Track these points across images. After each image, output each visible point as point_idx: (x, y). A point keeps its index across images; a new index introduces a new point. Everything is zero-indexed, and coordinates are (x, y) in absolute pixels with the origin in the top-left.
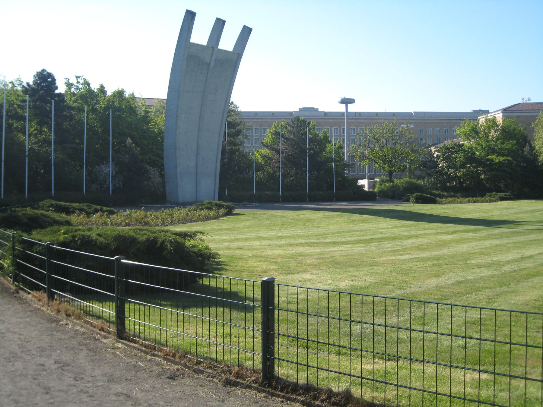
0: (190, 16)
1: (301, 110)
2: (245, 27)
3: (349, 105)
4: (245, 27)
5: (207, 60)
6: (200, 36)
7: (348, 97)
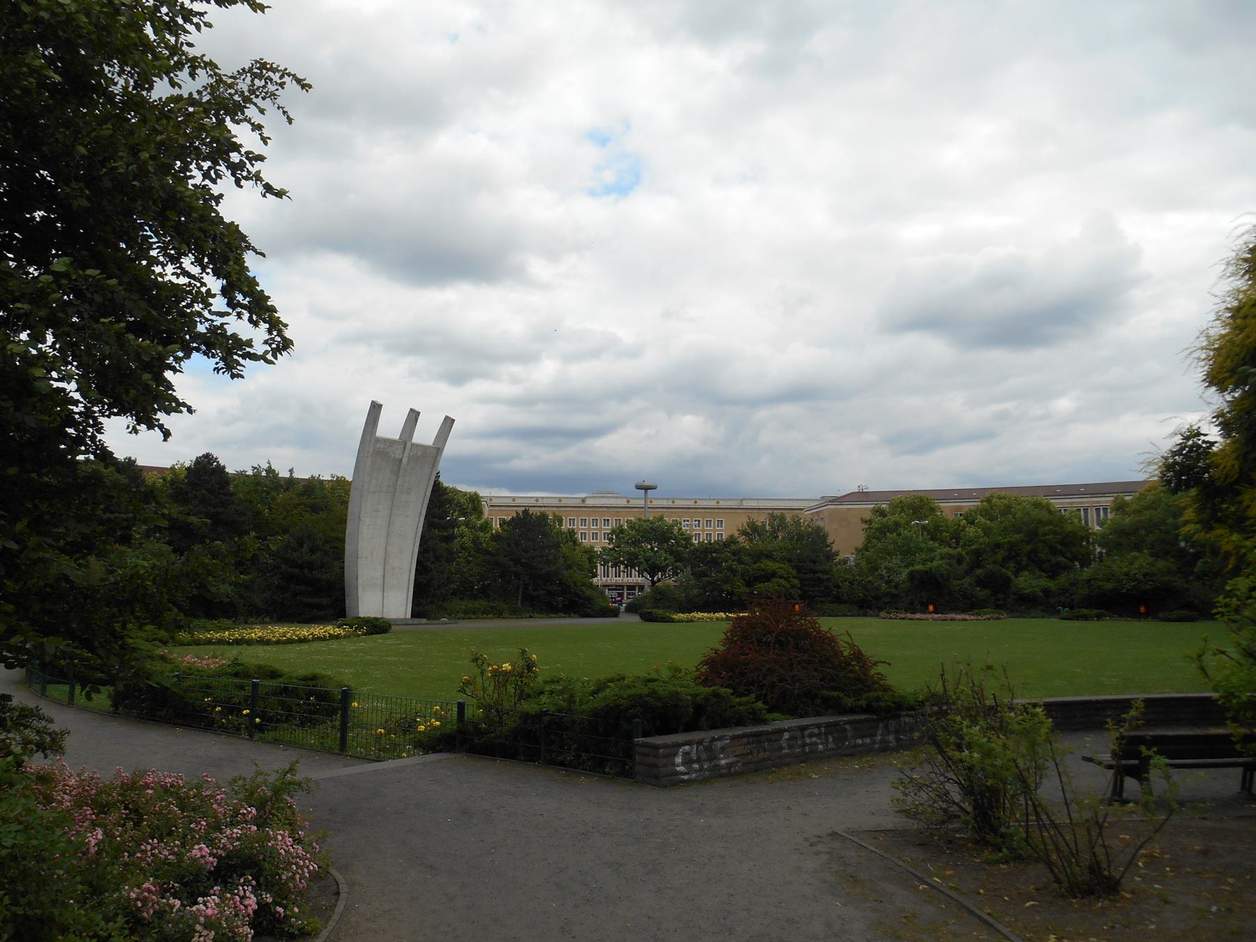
2: (447, 418)
4: (447, 418)
6: (390, 427)
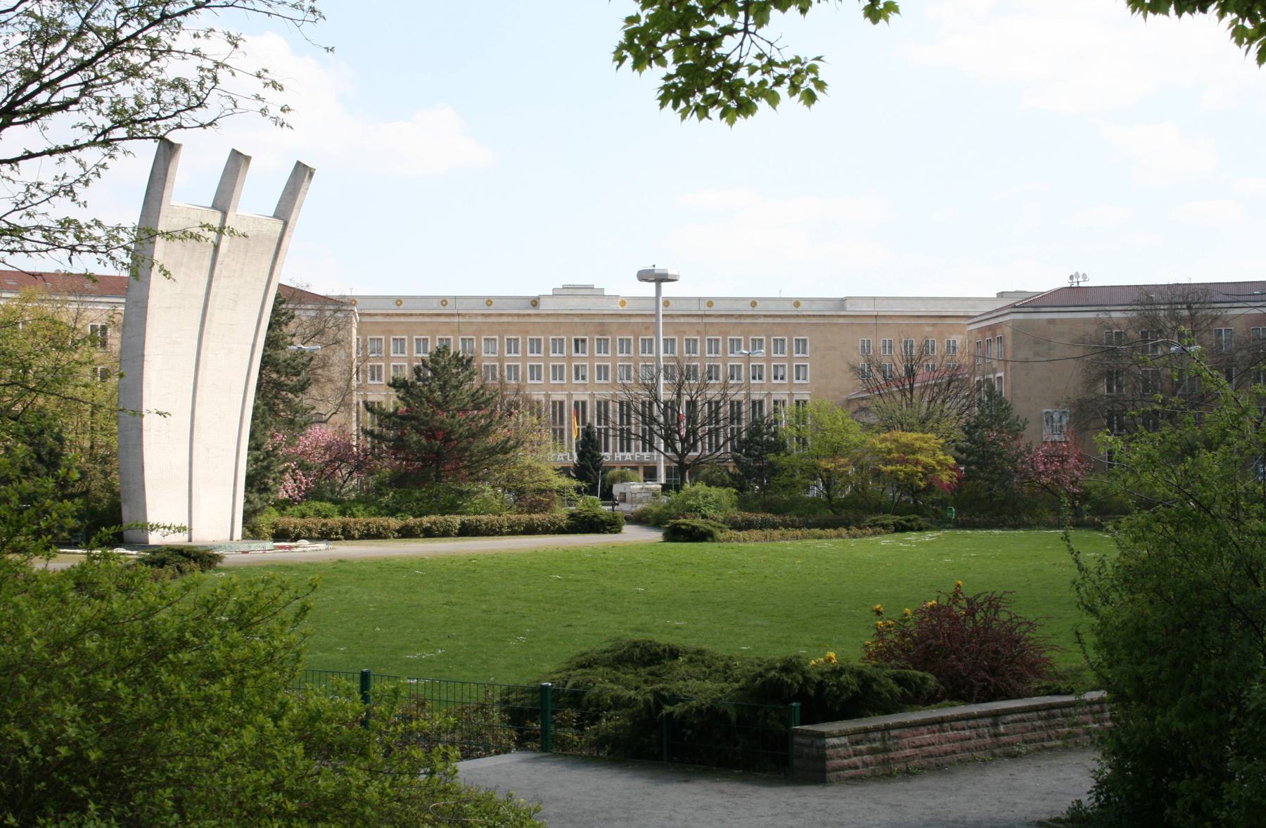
1: (556, 294)
3: (664, 285)
7: (660, 267)
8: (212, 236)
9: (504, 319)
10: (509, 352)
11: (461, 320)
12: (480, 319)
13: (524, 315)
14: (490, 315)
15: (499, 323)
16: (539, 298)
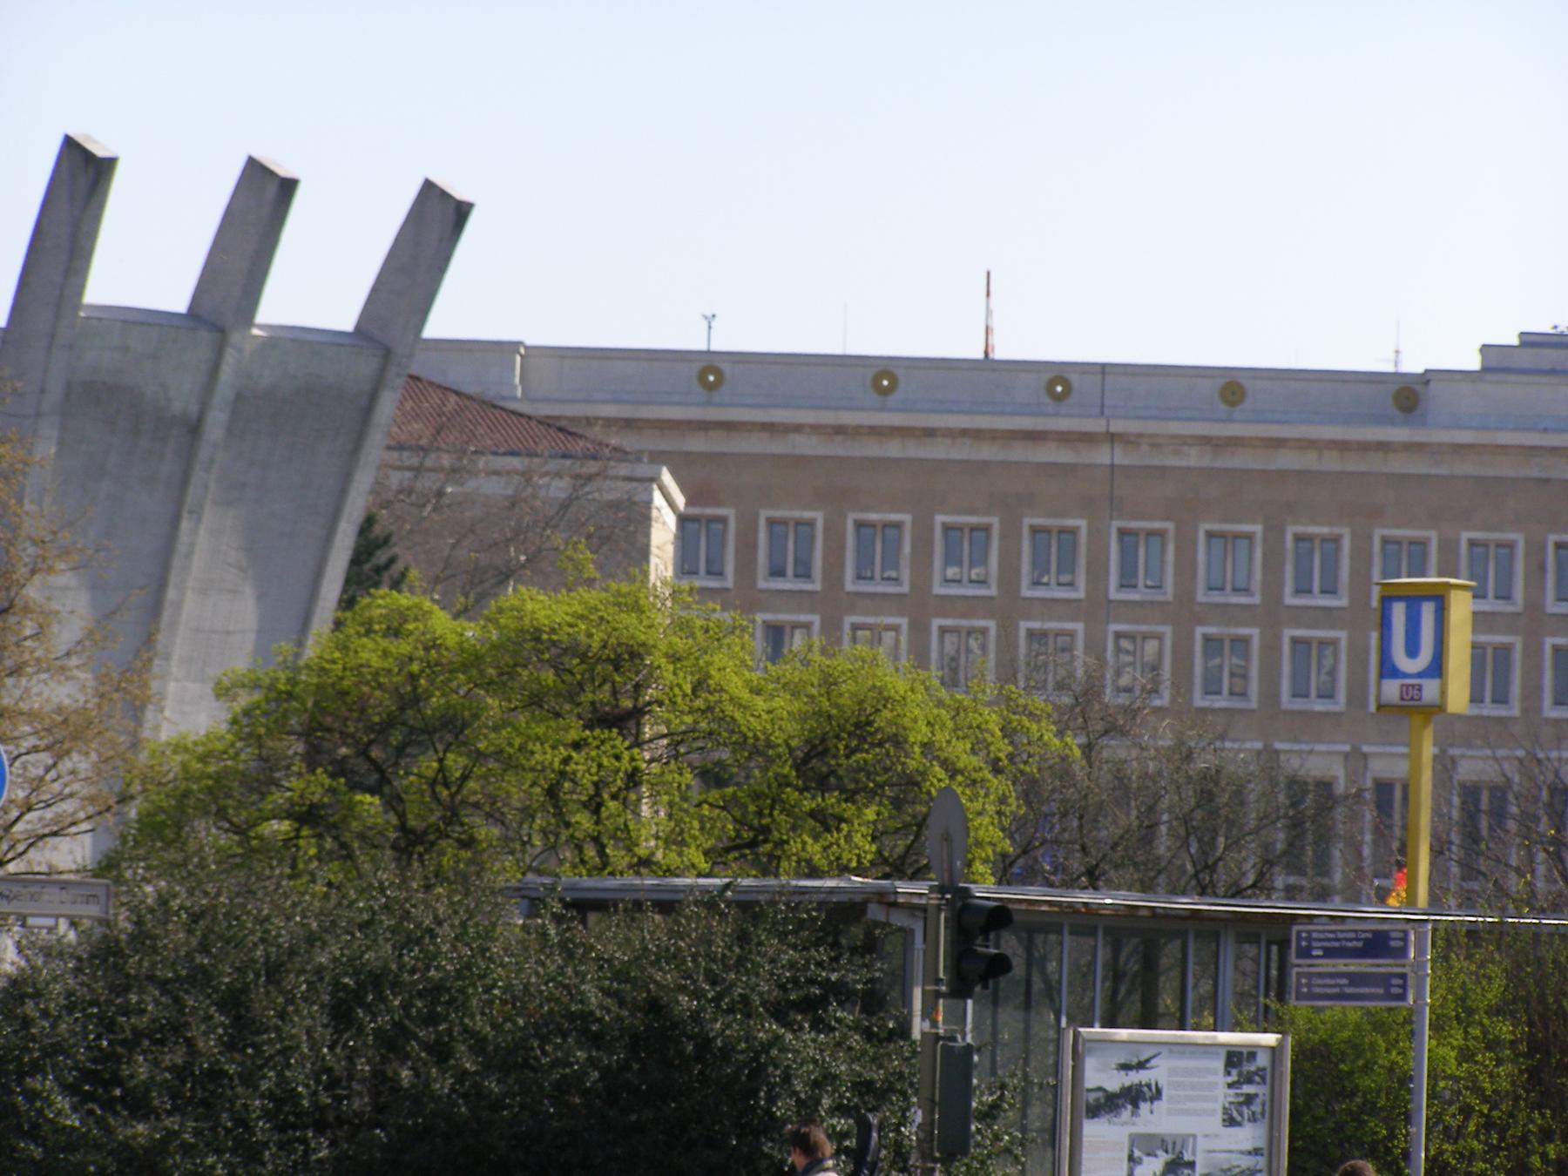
0: (82, 176)
5: (182, 400)
8: (241, 818)
9: (1287, 460)
10: (1302, 589)
11: (1121, 457)
12: (1194, 458)
13: (1365, 447)
14: (1234, 443)
15: (1268, 476)
16: (1428, 377)
